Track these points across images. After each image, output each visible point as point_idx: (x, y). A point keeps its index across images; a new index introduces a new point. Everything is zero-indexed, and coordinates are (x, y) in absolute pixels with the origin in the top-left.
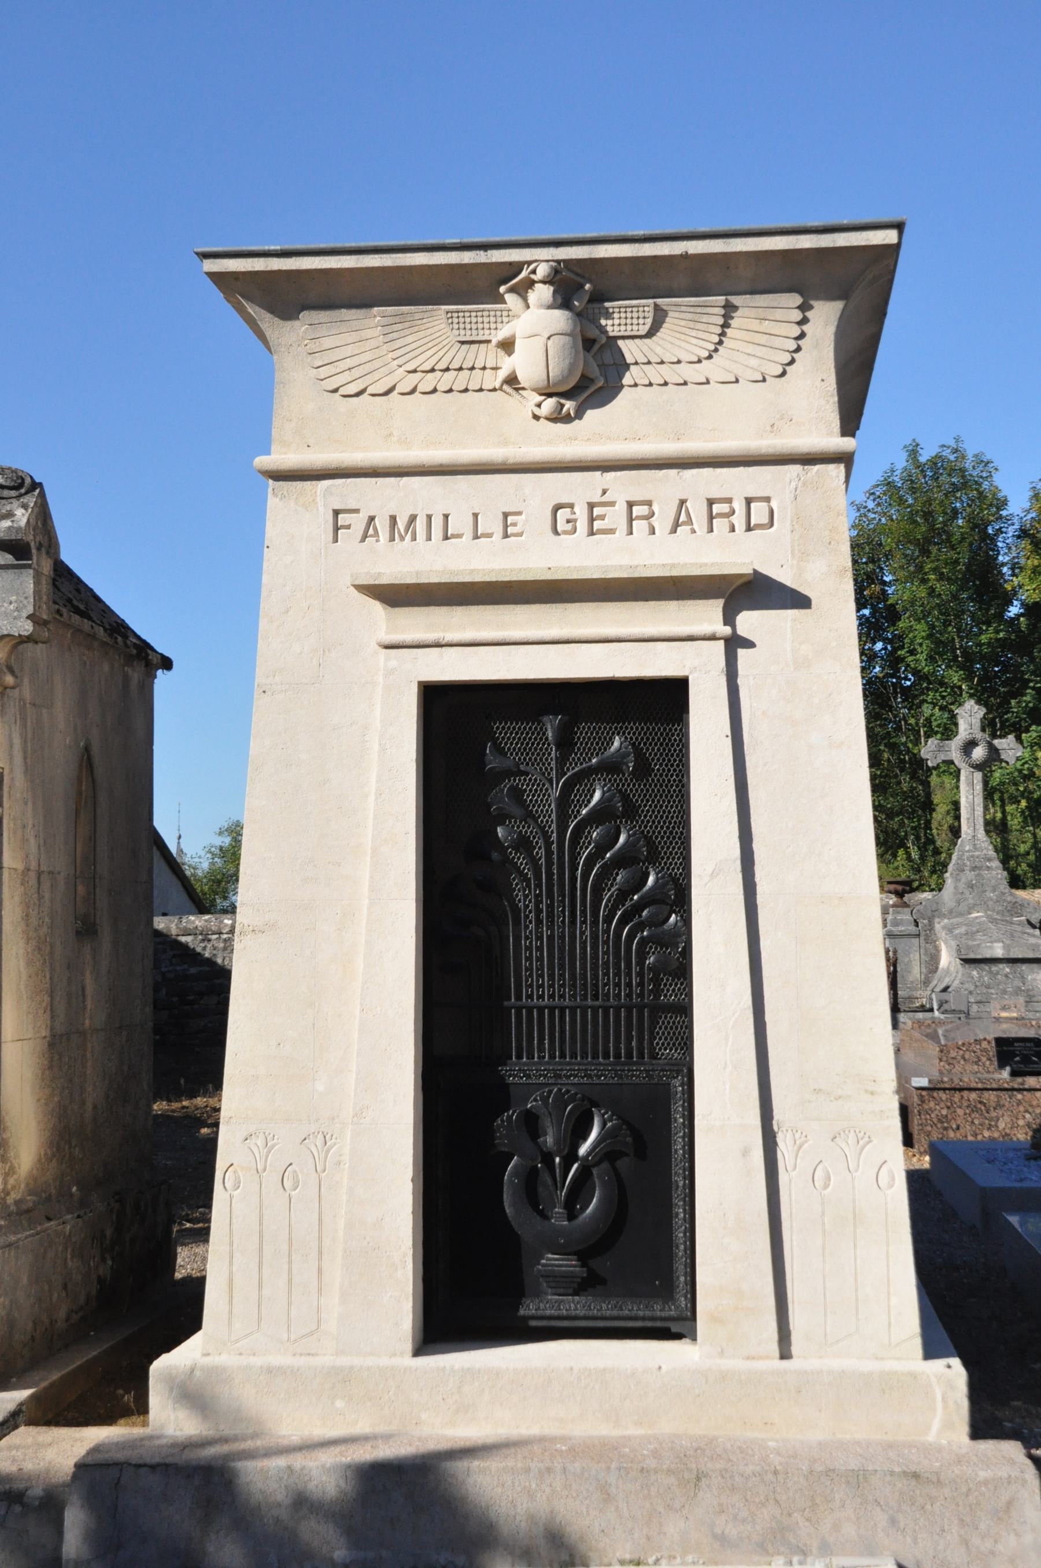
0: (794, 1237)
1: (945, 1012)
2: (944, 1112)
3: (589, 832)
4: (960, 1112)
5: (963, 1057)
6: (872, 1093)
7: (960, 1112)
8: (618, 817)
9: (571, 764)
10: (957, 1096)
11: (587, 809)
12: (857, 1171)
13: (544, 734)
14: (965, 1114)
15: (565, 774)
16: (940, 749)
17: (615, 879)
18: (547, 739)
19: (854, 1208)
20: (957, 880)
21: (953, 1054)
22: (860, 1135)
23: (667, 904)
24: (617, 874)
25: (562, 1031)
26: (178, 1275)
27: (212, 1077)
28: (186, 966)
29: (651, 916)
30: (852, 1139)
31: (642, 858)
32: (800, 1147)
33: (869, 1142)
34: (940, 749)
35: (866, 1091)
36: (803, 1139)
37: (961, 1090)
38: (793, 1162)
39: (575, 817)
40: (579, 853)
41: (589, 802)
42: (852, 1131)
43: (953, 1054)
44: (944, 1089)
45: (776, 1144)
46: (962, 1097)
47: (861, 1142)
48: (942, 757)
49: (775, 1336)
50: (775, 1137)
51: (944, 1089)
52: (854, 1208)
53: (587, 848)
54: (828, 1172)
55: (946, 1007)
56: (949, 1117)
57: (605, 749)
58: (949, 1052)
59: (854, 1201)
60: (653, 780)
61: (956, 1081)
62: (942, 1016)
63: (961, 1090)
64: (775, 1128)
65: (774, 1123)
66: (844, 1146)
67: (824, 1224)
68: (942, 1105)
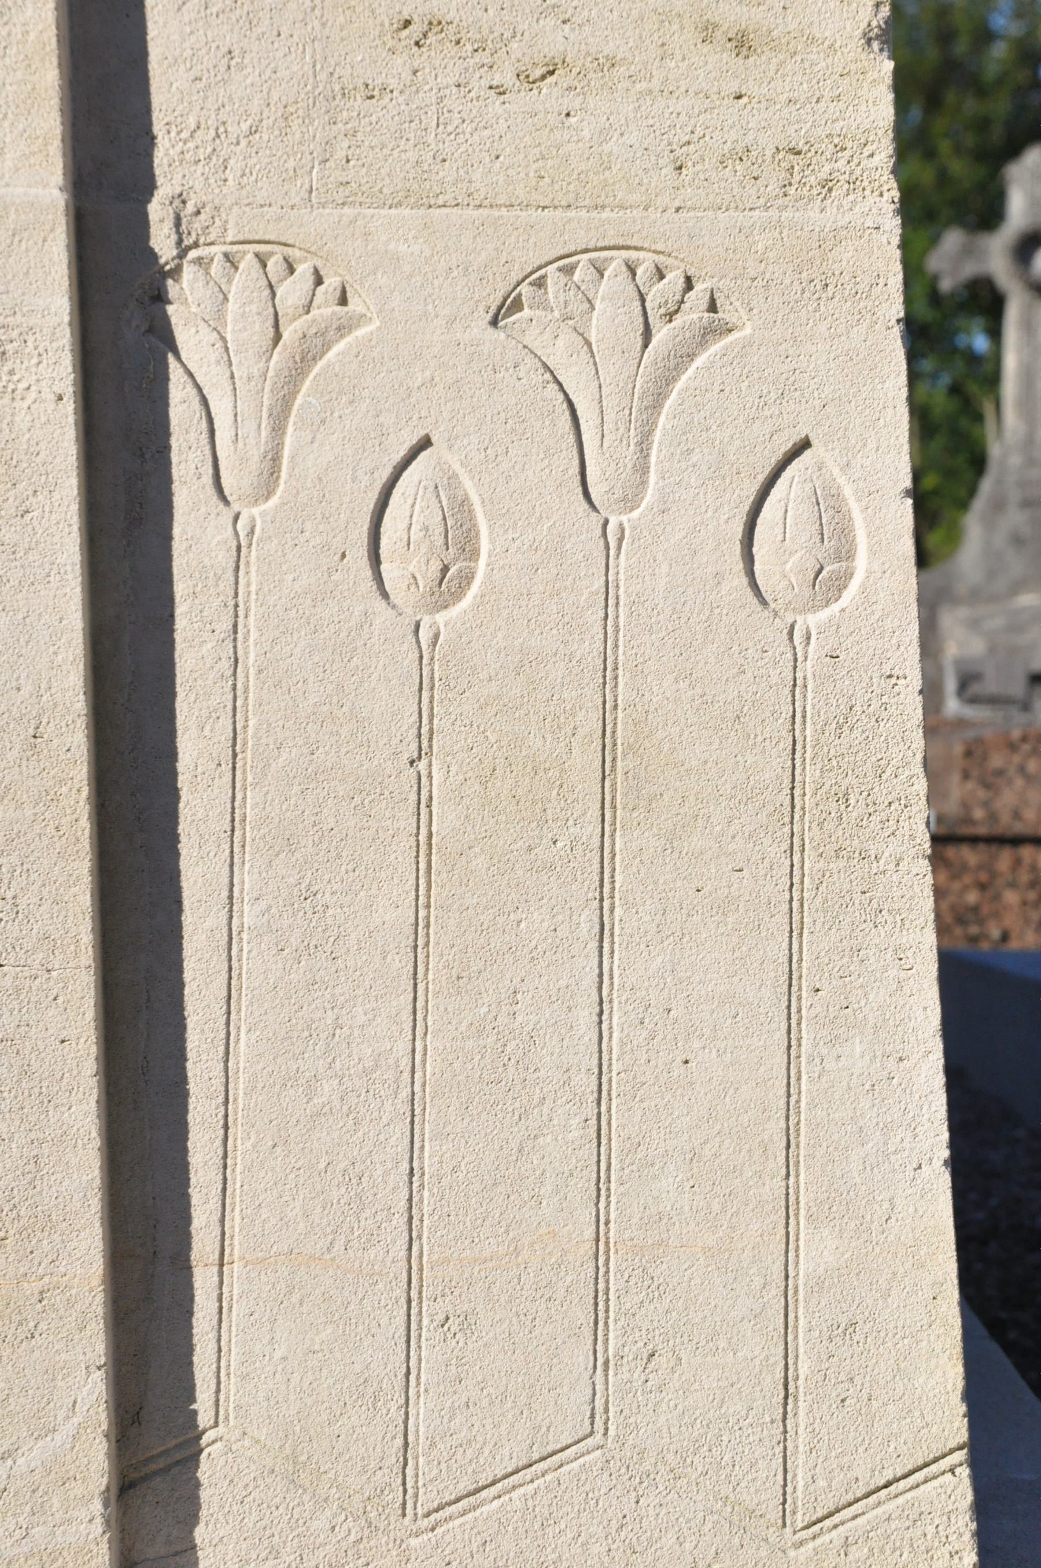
0: (247, 879)
1: (974, 700)
2: (972, 897)
4: (1011, 897)
5: (1022, 769)
6: (741, 44)
7: (1011, 897)
10: (1004, 858)
12: (630, 502)
14: (1024, 903)
16: (967, 252)
19: (606, 709)
20: (989, 526)
21: (996, 761)
22: (658, 294)
26: (192, 1407)
30: (611, 315)
32: (304, 360)
33: (710, 333)
34: (967, 252)
35: (708, 31)
36: (325, 310)
37: (1016, 841)
38: (256, 443)
42: (615, 266)
43: (996, 761)
44: (974, 840)
45: (162, 338)
46: (1018, 862)
47: (661, 334)
48: (970, 270)
49: (94, 1462)
50: (160, 298)
51: (974, 840)
52: (606, 709)
54: (464, 504)
55: (975, 688)
56: (985, 910)
58: (985, 758)
59: (607, 671)
61: (1005, 818)
62: (970, 712)
63: (1016, 841)
64: (162, 242)
65: (157, 210)
66: (560, 353)
67: (423, 804)
68: (967, 879)
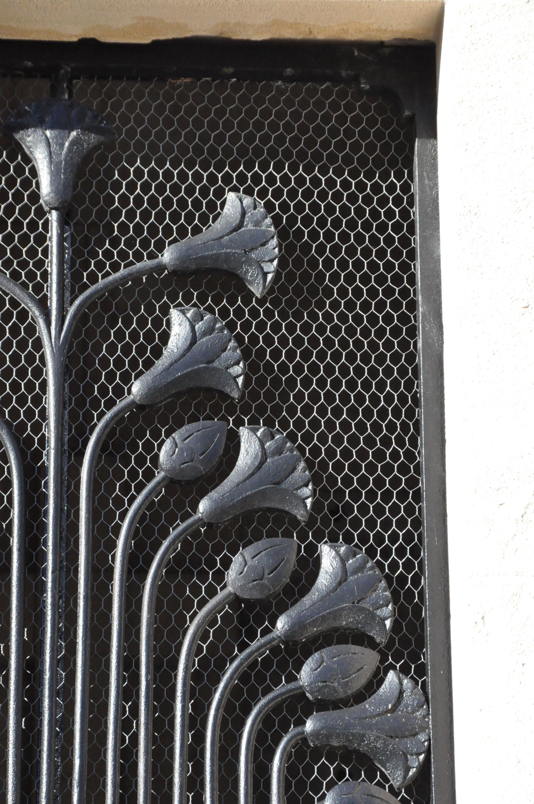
3: (148, 448)
8: (231, 410)
9: (100, 266)
11: (148, 377)
13: (27, 184)
15: (85, 287)
17: (220, 577)
18: (35, 197)
23: (372, 644)
24: (227, 563)
25: (65, 633)
27: (353, 643)
28: (293, 730)
29: (323, 676)
31: (300, 515)
39: (110, 404)
40: (119, 503)
41: (158, 353)
53: (140, 488)
57: (204, 220)
60: (328, 317)
